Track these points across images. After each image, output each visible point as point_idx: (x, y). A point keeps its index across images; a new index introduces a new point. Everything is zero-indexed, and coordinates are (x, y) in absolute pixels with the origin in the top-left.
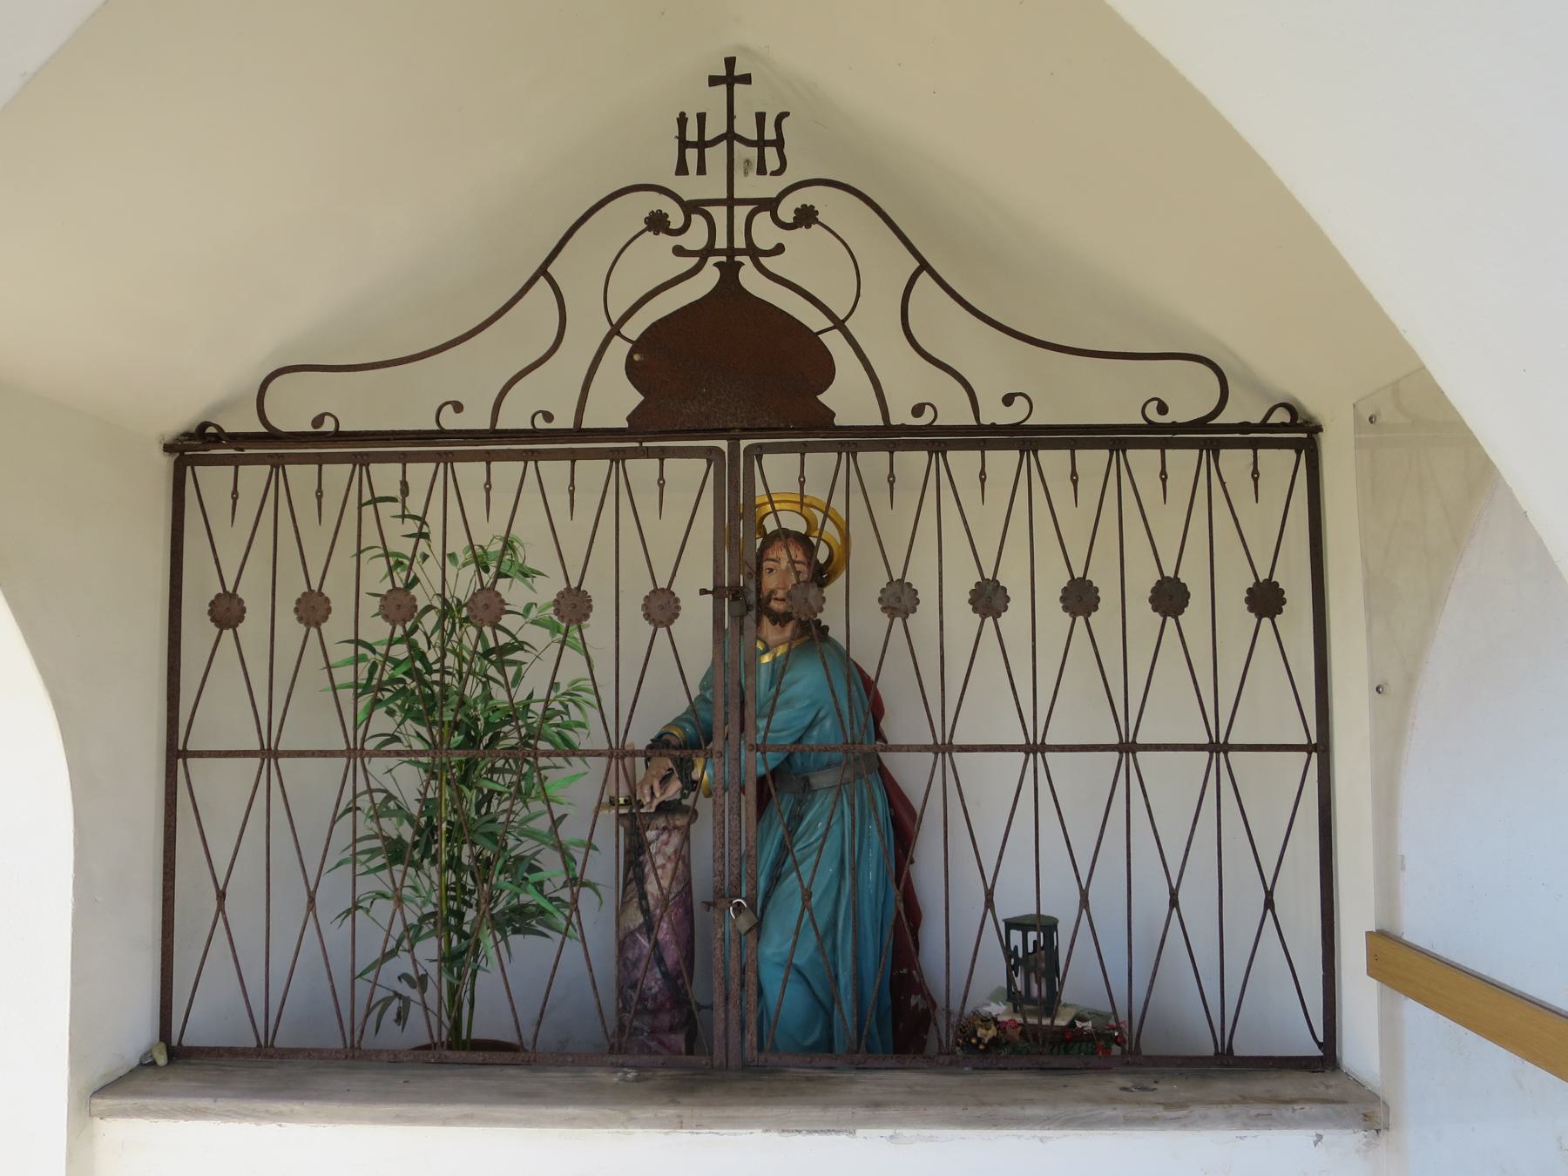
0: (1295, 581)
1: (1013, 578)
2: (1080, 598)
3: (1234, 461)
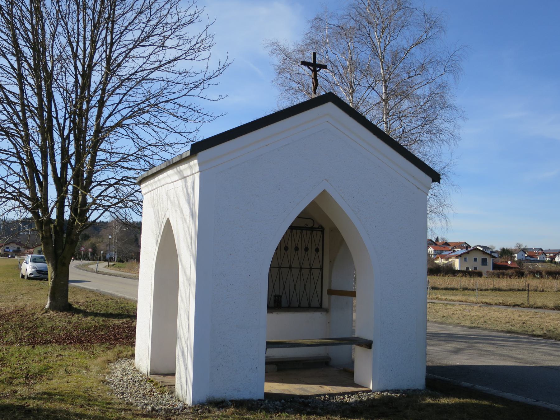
0: (320, 248)
1: (299, 246)
2: (306, 249)
3: (315, 232)
